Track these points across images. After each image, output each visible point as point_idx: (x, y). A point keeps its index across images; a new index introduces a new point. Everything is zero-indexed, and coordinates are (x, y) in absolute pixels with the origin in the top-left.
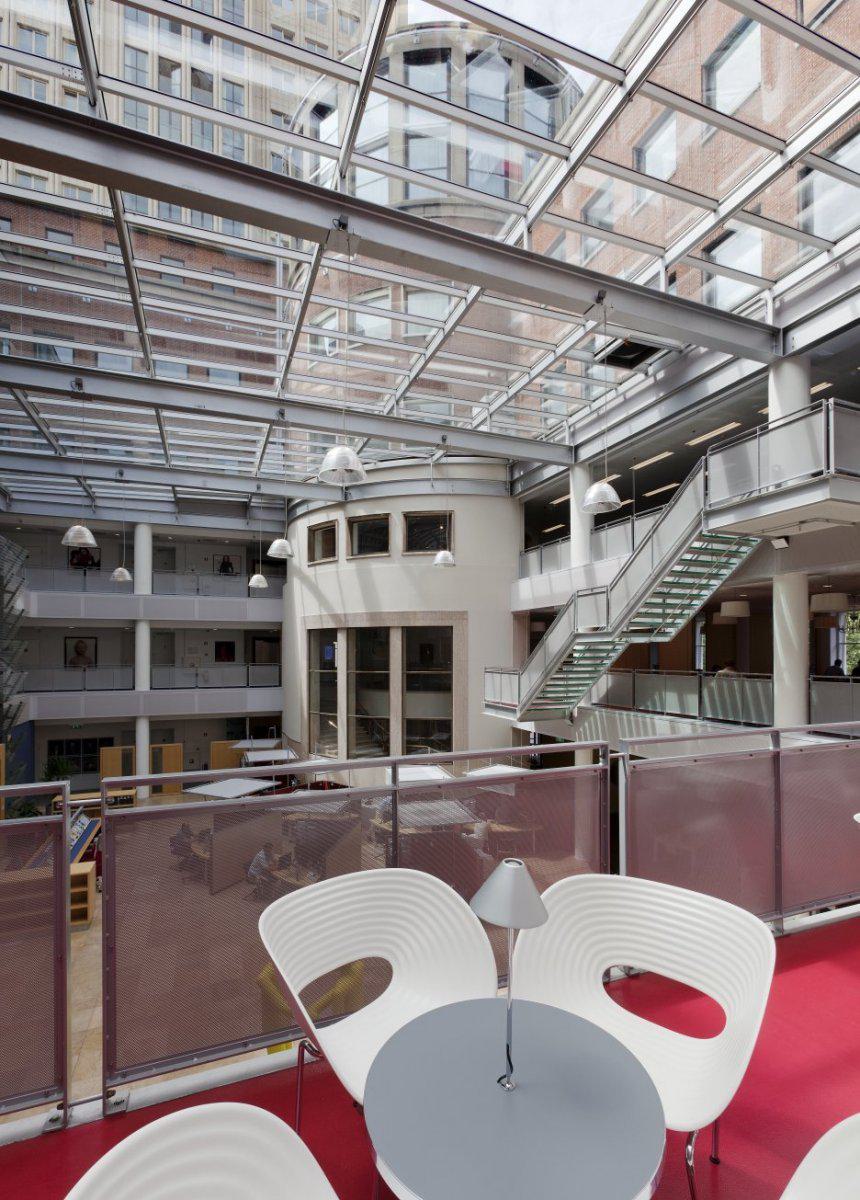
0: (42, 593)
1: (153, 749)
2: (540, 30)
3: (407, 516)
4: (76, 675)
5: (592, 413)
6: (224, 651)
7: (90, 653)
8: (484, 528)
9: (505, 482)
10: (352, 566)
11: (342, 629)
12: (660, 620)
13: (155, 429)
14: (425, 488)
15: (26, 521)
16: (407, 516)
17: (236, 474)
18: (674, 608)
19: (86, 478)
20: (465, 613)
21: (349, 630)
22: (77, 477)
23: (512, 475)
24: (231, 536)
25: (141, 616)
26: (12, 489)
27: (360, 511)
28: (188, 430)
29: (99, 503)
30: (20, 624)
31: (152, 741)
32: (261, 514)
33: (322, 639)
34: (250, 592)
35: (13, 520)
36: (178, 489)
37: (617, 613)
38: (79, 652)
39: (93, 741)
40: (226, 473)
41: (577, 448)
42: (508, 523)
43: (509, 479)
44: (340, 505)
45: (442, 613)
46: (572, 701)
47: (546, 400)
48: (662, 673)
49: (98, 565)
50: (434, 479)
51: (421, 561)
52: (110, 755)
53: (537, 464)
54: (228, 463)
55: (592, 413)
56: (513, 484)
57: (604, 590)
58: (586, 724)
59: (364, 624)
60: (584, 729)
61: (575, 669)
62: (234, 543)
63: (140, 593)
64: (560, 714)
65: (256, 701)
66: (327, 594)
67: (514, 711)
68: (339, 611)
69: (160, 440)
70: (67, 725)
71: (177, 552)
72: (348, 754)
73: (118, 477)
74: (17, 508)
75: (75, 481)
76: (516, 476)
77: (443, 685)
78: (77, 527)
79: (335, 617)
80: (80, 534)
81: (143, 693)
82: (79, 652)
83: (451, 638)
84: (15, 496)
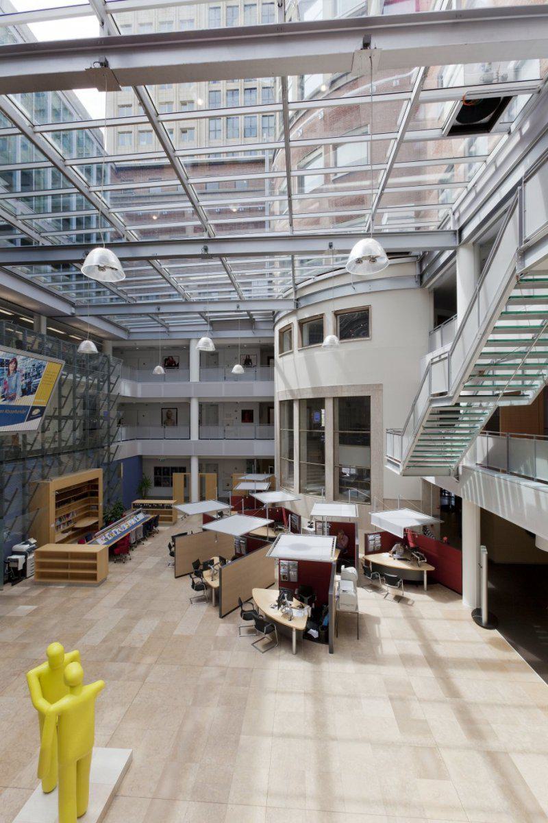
0: (144, 384)
1: (352, 499)
2: (72, 5)
3: (336, 314)
4: (169, 430)
5: (469, 193)
6: (247, 416)
7: (174, 418)
8: (398, 314)
9: (415, 276)
10: (302, 355)
11: (296, 400)
12: (520, 383)
13: (224, 275)
14: (349, 291)
15: (138, 344)
16: (336, 314)
17: (267, 298)
18: (516, 369)
19: (206, 312)
20: (381, 385)
21: (300, 400)
22: (199, 313)
23: (421, 268)
24: (244, 342)
25: (192, 395)
26: (129, 327)
27: (305, 314)
28: (258, 271)
29: (172, 329)
30: (119, 401)
31: (200, 471)
32: (262, 326)
33: (289, 404)
34: (237, 377)
35: (132, 344)
36: (252, 313)
37: (456, 375)
38: (169, 417)
39: (168, 468)
40: (232, 299)
41: (461, 230)
42: (422, 307)
43: (418, 272)
44: (294, 312)
45: (362, 386)
46: (455, 460)
47: (443, 191)
48: (532, 438)
49: (178, 365)
50: (354, 283)
51: (355, 346)
52: (178, 478)
53: (437, 252)
54: (213, 294)
55: (469, 193)
56: (421, 276)
57: (447, 355)
58: (468, 483)
59: (310, 396)
60: (467, 485)
61: (457, 432)
62: (250, 347)
63: (194, 384)
64: (445, 471)
65: (259, 449)
66: (296, 374)
67: (398, 466)
68: (294, 387)
69: (230, 282)
70: (157, 459)
71: (220, 355)
72: (300, 489)
73: (157, 312)
74: (175, 336)
75: (198, 315)
76: (424, 268)
77: (365, 441)
78: (87, 341)
79: (291, 391)
80: (88, 346)
81: (193, 443)
82: (169, 417)
83: (369, 406)
84: (132, 331)
